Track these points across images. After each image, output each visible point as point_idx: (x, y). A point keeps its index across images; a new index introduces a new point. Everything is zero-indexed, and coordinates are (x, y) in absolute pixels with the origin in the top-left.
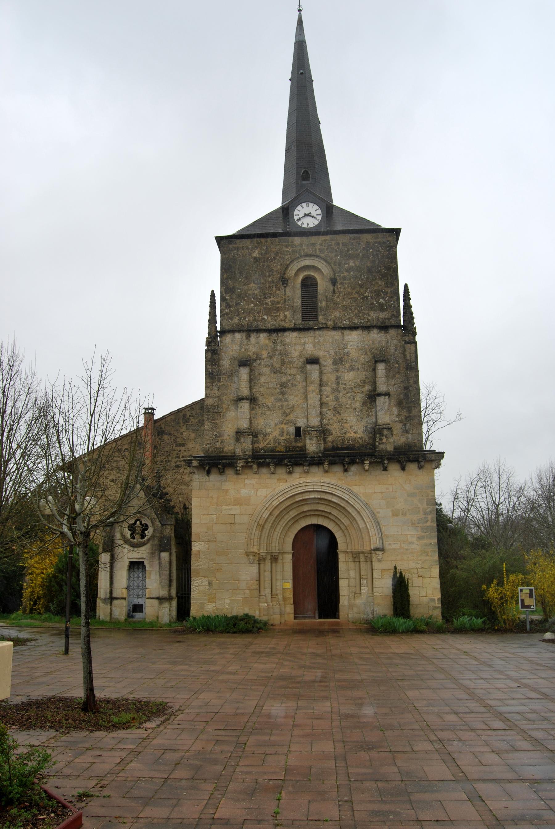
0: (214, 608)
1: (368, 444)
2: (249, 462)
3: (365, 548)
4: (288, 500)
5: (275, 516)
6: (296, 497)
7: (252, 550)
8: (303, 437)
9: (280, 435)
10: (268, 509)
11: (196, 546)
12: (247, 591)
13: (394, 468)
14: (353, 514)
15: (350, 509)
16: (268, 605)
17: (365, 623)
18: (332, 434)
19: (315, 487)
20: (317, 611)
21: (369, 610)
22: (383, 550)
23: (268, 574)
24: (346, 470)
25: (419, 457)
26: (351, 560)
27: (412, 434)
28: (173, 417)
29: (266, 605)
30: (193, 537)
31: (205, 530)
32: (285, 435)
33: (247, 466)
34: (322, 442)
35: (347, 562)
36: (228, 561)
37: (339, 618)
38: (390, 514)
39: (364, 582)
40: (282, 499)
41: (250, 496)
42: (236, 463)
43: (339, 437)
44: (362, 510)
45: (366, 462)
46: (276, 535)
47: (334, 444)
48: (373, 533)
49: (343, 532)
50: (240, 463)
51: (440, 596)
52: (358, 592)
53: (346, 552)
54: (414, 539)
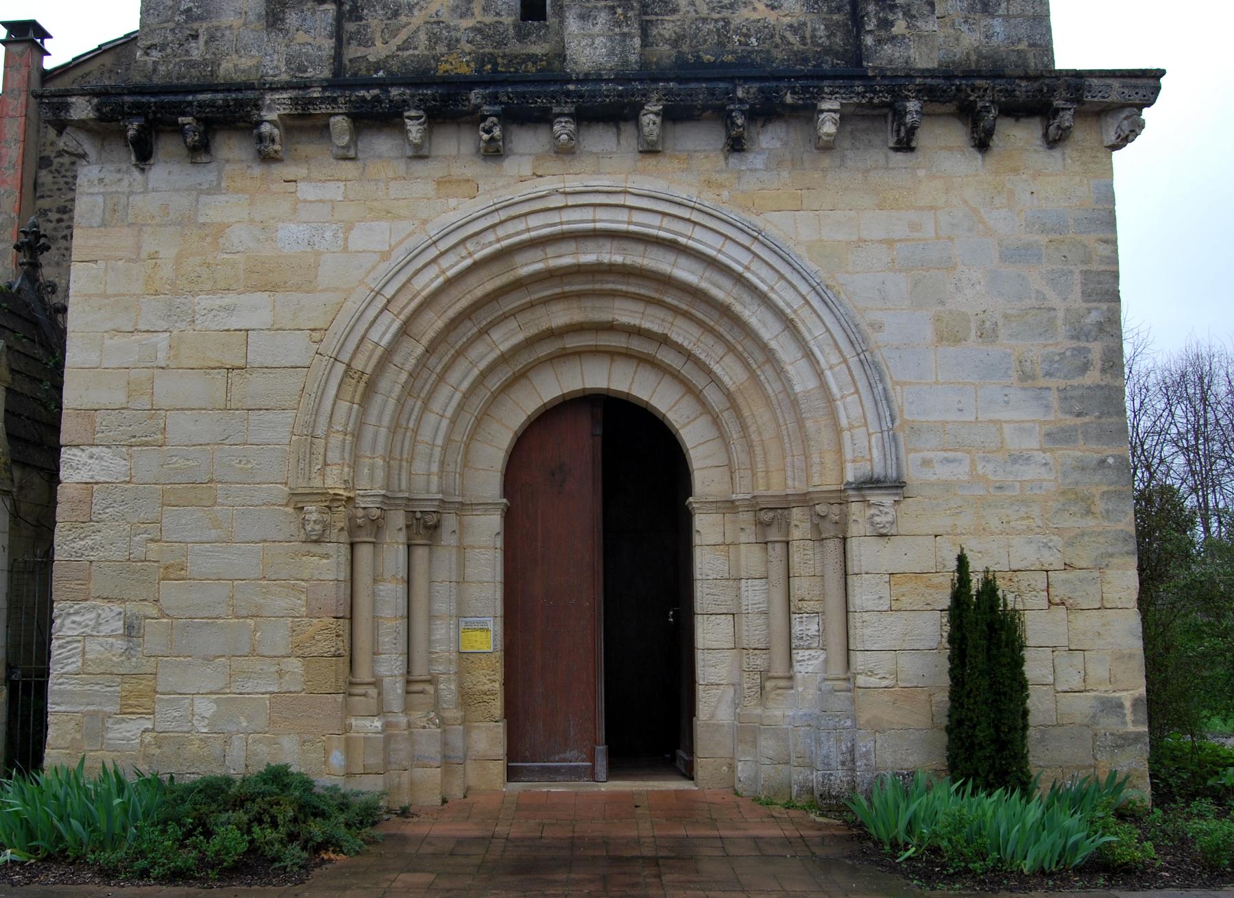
0: (148, 738)
1: (828, 51)
2: (312, 101)
3: (816, 480)
4: (484, 273)
5: (425, 341)
6: (519, 259)
7: (317, 482)
8: (552, 20)
9: (454, 9)
10: (395, 308)
11: (78, 467)
12: (295, 665)
13: (944, 144)
14: (766, 335)
15: (752, 314)
16: (387, 725)
17: (812, 806)
18: (674, 11)
19: (601, 214)
20: (601, 749)
21: (833, 750)
22: (897, 486)
23: (392, 591)
24: (736, 145)
25: (1052, 90)
26: (749, 536)
27: (1007, 17)
28: (107, 60)
29: (378, 723)
30: (69, 428)
31: (119, 398)
32: (477, 10)
33: (306, 122)
34: (635, 29)
35: (728, 545)
36: (214, 534)
37: (690, 776)
38: (929, 333)
39: (806, 627)
40: (454, 264)
41: (318, 254)
42: (258, 107)
43: (704, 20)
44: (805, 313)
45: (825, 105)
46: (434, 426)
47: (685, 48)
48: (856, 412)
49: (716, 421)
50: (273, 112)
51: (1142, 691)
52: (779, 669)
53: (729, 506)
54: (1032, 443)
